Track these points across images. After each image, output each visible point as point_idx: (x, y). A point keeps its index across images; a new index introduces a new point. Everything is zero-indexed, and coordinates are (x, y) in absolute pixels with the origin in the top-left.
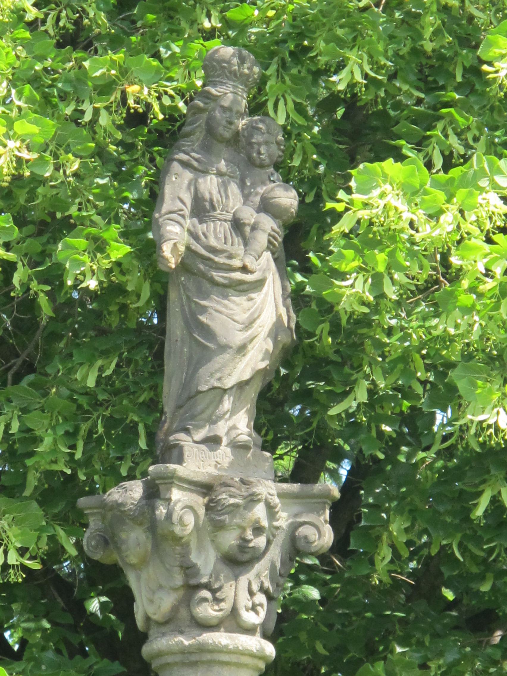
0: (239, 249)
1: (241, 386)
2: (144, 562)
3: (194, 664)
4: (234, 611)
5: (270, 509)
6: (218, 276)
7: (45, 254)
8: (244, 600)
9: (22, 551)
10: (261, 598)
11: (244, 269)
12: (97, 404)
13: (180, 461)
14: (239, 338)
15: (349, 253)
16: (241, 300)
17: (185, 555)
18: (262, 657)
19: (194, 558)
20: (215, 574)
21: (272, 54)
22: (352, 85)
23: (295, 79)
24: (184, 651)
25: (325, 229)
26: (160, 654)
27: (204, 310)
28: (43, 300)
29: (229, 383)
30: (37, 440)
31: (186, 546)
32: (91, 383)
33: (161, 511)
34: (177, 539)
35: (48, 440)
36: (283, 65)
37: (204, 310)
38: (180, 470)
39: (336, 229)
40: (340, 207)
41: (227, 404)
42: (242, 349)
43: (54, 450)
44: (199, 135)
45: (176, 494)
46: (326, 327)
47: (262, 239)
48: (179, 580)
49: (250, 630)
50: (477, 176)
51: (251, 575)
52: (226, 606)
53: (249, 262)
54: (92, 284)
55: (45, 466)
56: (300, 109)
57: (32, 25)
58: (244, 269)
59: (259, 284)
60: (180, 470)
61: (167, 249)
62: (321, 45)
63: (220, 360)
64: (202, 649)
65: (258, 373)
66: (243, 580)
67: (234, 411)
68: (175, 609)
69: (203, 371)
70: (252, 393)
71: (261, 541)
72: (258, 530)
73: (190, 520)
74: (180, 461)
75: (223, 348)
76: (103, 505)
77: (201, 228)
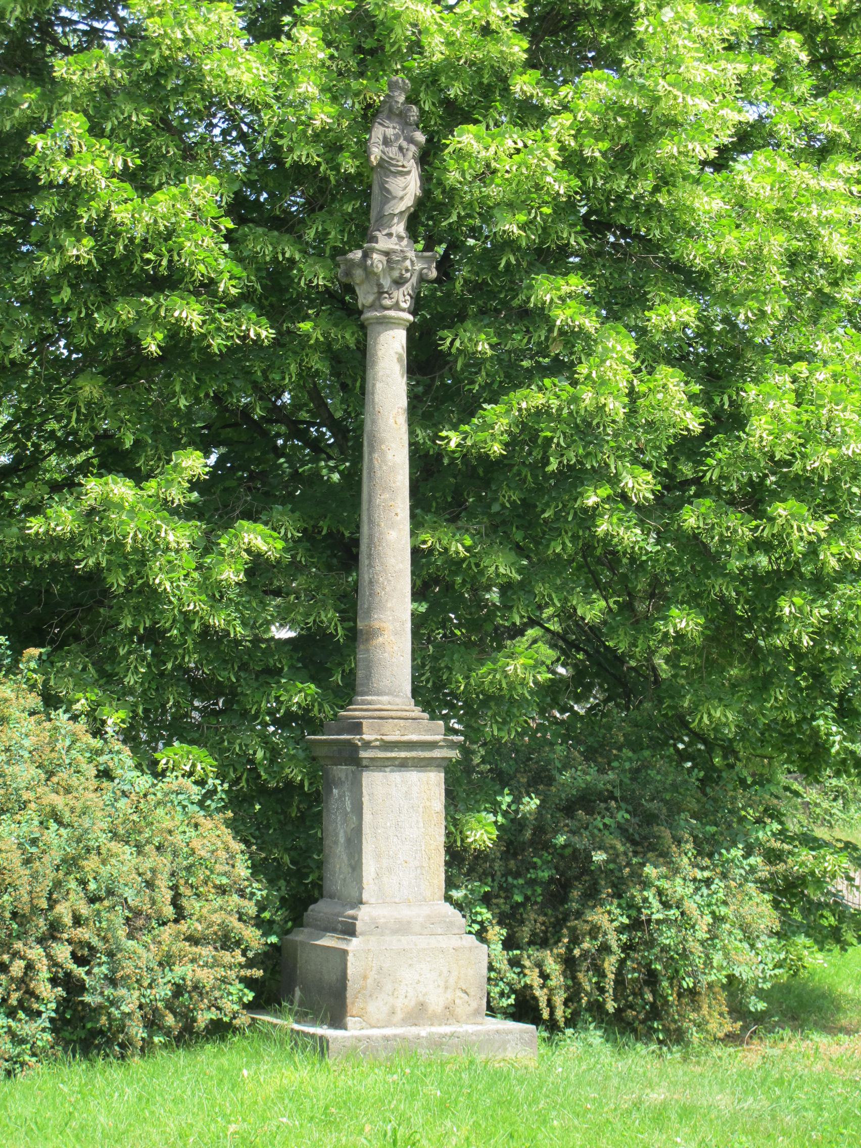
0: (401, 158)
1: (401, 213)
2: (362, 282)
3: (381, 323)
4: (397, 303)
5: (412, 262)
6: (392, 169)
7: (333, 160)
8: (401, 298)
9: (324, 278)
10: (408, 298)
11: (403, 166)
12: (352, 220)
13: (377, 242)
14: (401, 194)
15: (452, 162)
16: (402, 178)
17: (378, 280)
18: (408, 321)
19: (381, 281)
20: (390, 287)
21: (423, 82)
22: (456, 96)
23: (433, 92)
24: (377, 318)
25: (442, 151)
26: (368, 319)
27: (387, 182)
28: (332, 178)
29: (397, 211)
30: (329, 233)
31: (379, 277)
32: (350, 210)
33: (369, 262)
34: (375, 274)
35: (333, 233)
36: (427, 86)
37: (387, 182)
38: (376, 246)
39: (446, 151)
40: (448, 142)
41: (396, 220)
42: (402, 198)
43: (336, 237)
44: (386, 113)
45: (375, 256)
46: (439, 190)
47: (410, 154)
48: (376, 290)
49: (403, 310)
50: (504, 133)
51: (404, 288)
52: (394, 300)
53: (405, 163)
54: (352, 171)
55: (332, 244)
56: (434, 104)
57: (328, 68)
58: (403, 166)
59: (409, 172)
60: (376, 246)
61: (372, 158)
62: (443, 79)
63: (393, 202)
64: (385, 317)
65: (409, 208)
66: (401, 290)
67: (398, 223)
68: (374, 301)
69: (386, 207)
70: (406, 215)
71: (408, 275)
72: (407, 270)
73: (380, 266)
74: (377, 242)
75: (395, 198)
76: (346, 260)
77: (386, 149)
